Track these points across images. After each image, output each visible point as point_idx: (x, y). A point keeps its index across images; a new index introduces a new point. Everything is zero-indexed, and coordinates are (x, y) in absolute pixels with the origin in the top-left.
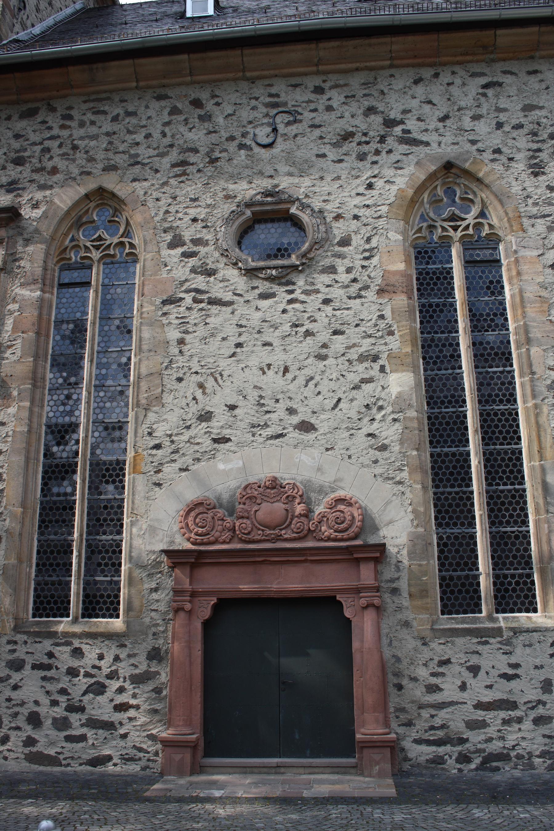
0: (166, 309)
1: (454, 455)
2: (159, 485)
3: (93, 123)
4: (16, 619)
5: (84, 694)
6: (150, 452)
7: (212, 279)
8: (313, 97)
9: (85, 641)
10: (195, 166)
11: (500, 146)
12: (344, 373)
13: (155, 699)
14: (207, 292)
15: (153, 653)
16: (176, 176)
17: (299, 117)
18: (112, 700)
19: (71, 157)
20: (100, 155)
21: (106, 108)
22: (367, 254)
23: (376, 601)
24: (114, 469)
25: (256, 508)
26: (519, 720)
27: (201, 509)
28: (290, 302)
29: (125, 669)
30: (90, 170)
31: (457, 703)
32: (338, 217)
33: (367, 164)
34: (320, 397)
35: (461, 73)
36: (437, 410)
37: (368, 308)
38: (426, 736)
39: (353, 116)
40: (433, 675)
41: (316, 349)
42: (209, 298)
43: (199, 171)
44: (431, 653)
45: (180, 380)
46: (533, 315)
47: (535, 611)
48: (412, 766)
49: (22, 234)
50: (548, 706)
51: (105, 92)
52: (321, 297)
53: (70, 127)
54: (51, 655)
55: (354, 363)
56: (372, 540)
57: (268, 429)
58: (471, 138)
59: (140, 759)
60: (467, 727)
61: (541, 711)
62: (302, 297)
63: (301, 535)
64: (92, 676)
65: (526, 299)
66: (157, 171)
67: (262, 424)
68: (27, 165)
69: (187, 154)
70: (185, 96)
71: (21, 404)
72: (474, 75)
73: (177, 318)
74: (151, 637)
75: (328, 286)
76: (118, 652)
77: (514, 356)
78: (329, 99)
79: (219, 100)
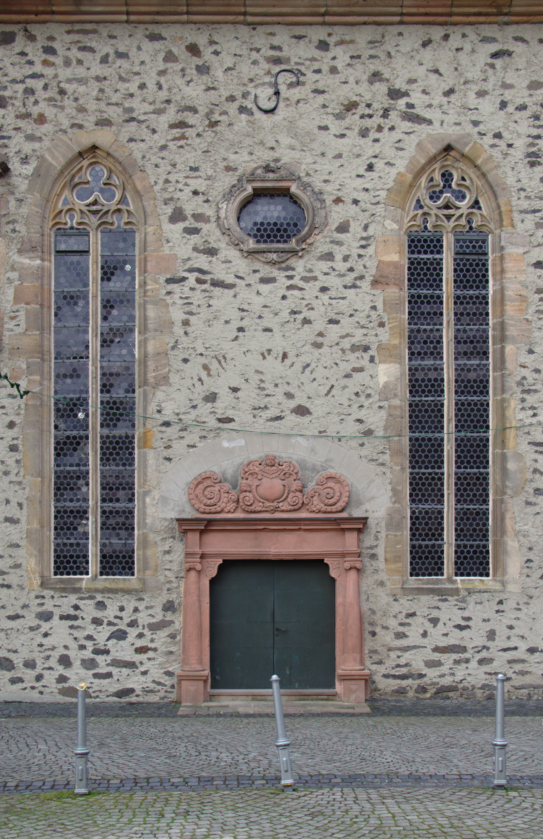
0: (170, 287)
1: (430, 440)
2: (169, 459)
3: (80, 62)
4: (42, 577)
5: (108, 640)
6: (160, 428)
7: (214, 259)
8: (317, 54)
9: (107, 595)
10: (194, 129)
11: (501, 130)
12: (337, 362)
13: (170, 643)
14: (210, 273)
15: (168, 605)
16: (174, 139)
17: (302, 79)
18: (133, 644)
19: (59, 103)
20: (92, 106)
21: (93, 44)
22: (363, 243)
23: (358, 565)
24: (124, 443)
25: (257, 483)
26: (467, 661)
27: (208, 482)
28: (289, 288)
29: (143, 618)
30: (81, 123)
31: (419, 647)
32: (338, 200)
33: (368, 141)
34: (315, 383)
35: (472, 36)
36: (417, 399)
37: (363, 299)
38: (393, 672)
39: (357, 83)
40: (401, 624)
41: (313, 338)
42: (212, 279)
43: (198, 135)
44: (400, 607)
45: (186, 361)
46: (512, 313)
47: (487, 575)
48: (380, 695)
49: (13, 193)
50: (490, 651)
51: (91, 22)
52: (319, 284)
53: (54, 64)
54: (76, 607)
55: (347, 352)
56: (357, 513)
57: (267, 412)
58: (473, 118)
59: (159, 691)
60: (426, 666)
61: (484, 654)
62: (301, 284)
63: (296, 507)
64: (115, 625)
65: (507, 298)
66: (154, 131)
67: (262, 406)
68: (10, 108)
69: (185, 113)
70: (181, 38)
71: (31, 377)
72: (485, 40)
73: (181, 298)
74: (165, 592)
75: (326, 274)
76: (137, 604)
77: (491, 350)
78: (334, 58)
79: (218, 48)
